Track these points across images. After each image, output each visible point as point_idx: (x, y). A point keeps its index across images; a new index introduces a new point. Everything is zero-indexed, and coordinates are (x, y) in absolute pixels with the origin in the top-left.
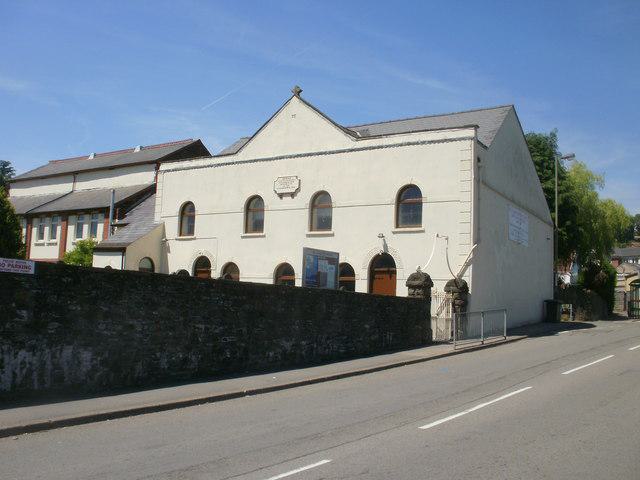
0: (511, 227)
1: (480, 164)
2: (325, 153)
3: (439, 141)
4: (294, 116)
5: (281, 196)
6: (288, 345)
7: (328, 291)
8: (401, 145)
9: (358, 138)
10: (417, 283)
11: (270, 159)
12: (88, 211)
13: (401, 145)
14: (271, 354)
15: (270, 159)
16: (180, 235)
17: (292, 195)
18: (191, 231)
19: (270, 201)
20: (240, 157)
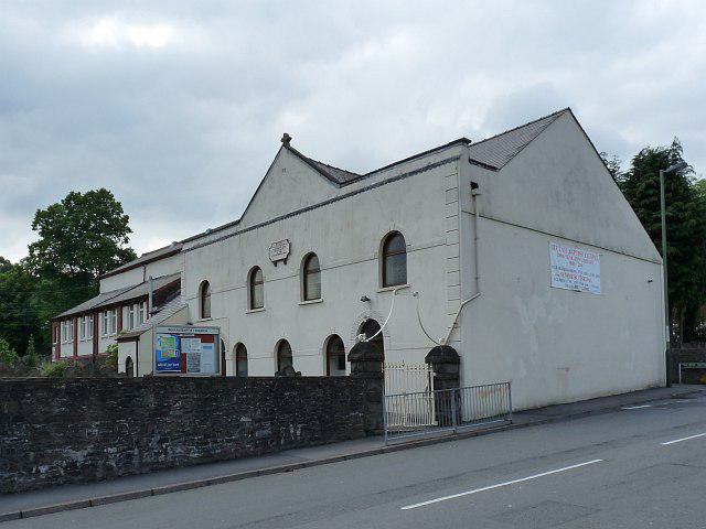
0: (554, 272)
1: (476, 191)
2: (311, 208)
3: (420, 171)
4: (284, 170)
5: (275, 263)
6: (79, 456)
7: (199, 382)
8: (382, 184)
9: (342, 185)
10: (357, 356)
11: (265, 224)
12: (121, 304)
13: (382, 184)
14: (43, 469)
15: (265, 224)
16: (253, 308)
17: (285, 261)
18: (401, 280)
19: (267, 271)
20: (242, 227)
